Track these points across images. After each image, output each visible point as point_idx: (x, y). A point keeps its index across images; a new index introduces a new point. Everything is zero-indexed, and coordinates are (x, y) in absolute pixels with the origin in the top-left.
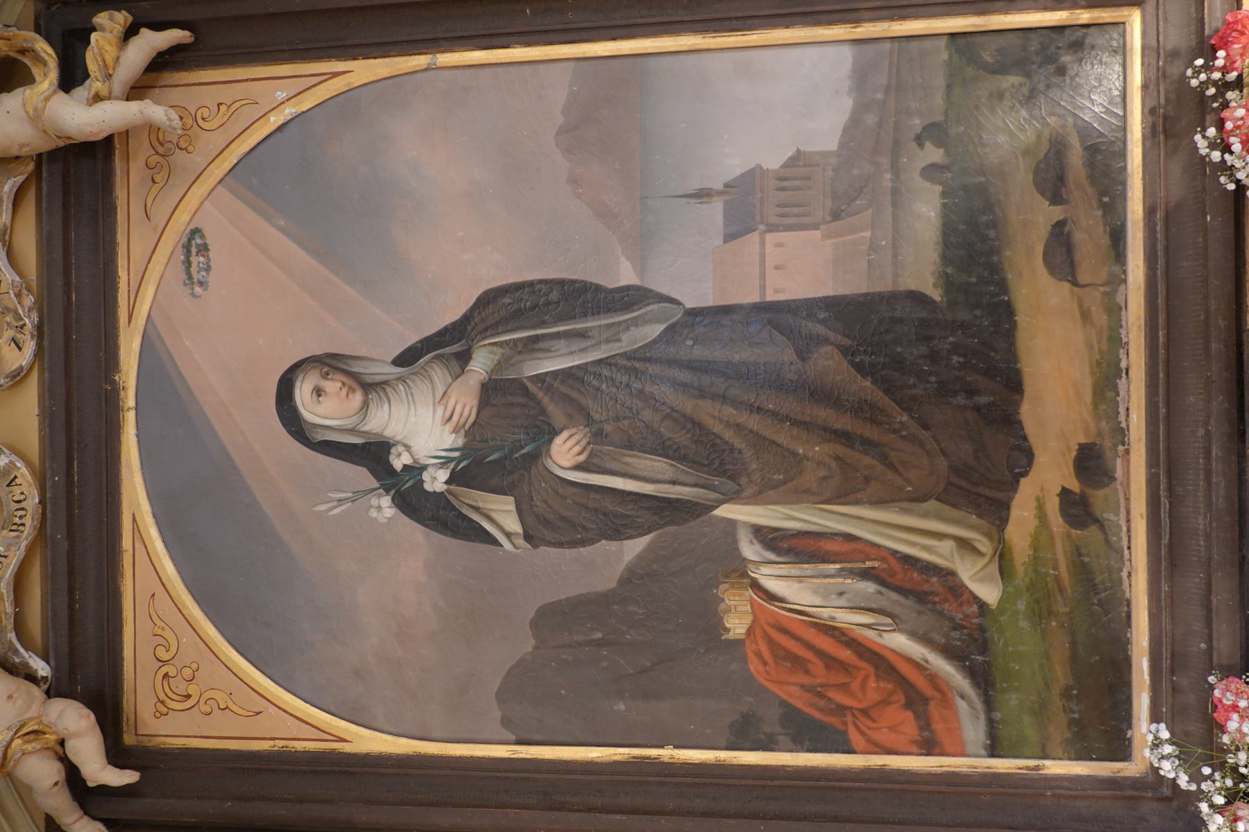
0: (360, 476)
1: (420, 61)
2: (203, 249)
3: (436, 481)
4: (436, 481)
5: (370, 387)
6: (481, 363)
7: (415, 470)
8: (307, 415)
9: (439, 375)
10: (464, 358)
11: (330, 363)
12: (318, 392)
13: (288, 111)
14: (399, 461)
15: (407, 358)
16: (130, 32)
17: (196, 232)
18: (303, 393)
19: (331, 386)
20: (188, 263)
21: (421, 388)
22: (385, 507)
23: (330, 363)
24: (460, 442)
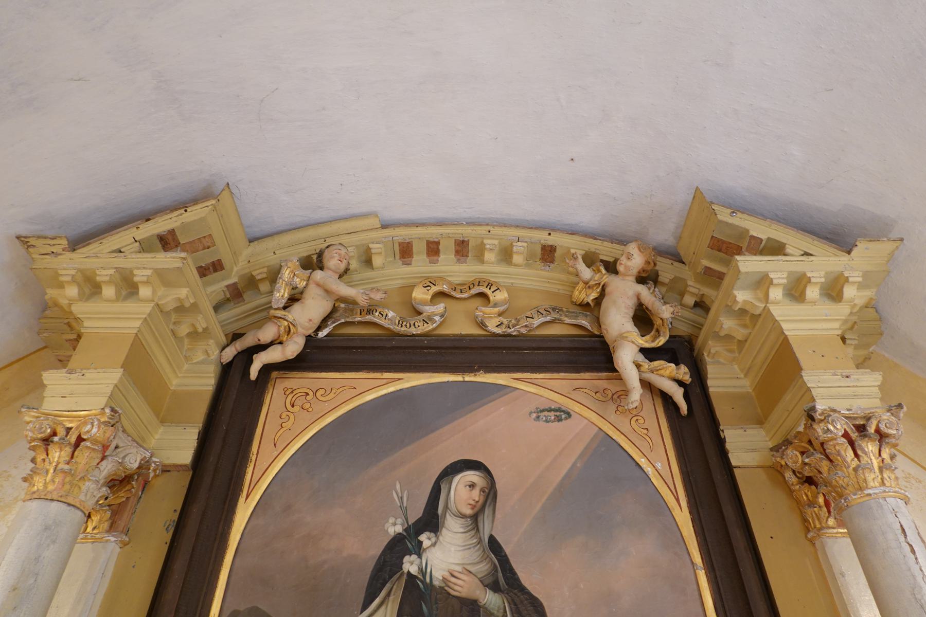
0: (416, 512)
1: (697, 559)
2: (559, 419)
3: (410, 565)
4: (410, 565)
5: (475, 519)
6: (491, 600)
7: (418, 550)
8: (457, 479)
9: (483, 568)
10: (494, 587)
11: (491, 493)
12: (472, 486)
13: (649, 470)
14: (425, 539)
15: (494, 546)
16: (680, 383)
17: (569, 415)
18: (471, 476)
19: (476, 494)
20: (550, 410)
21: (474, 555)
22: (395, 528)
23: (491, 493)
24: (436, 583)
